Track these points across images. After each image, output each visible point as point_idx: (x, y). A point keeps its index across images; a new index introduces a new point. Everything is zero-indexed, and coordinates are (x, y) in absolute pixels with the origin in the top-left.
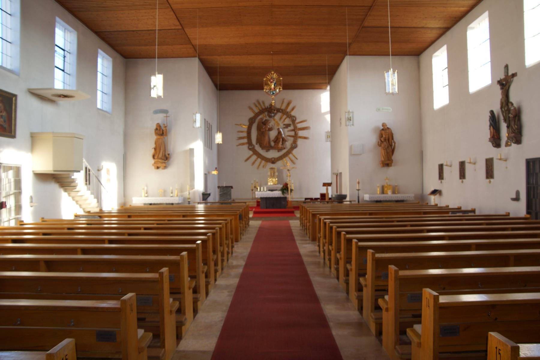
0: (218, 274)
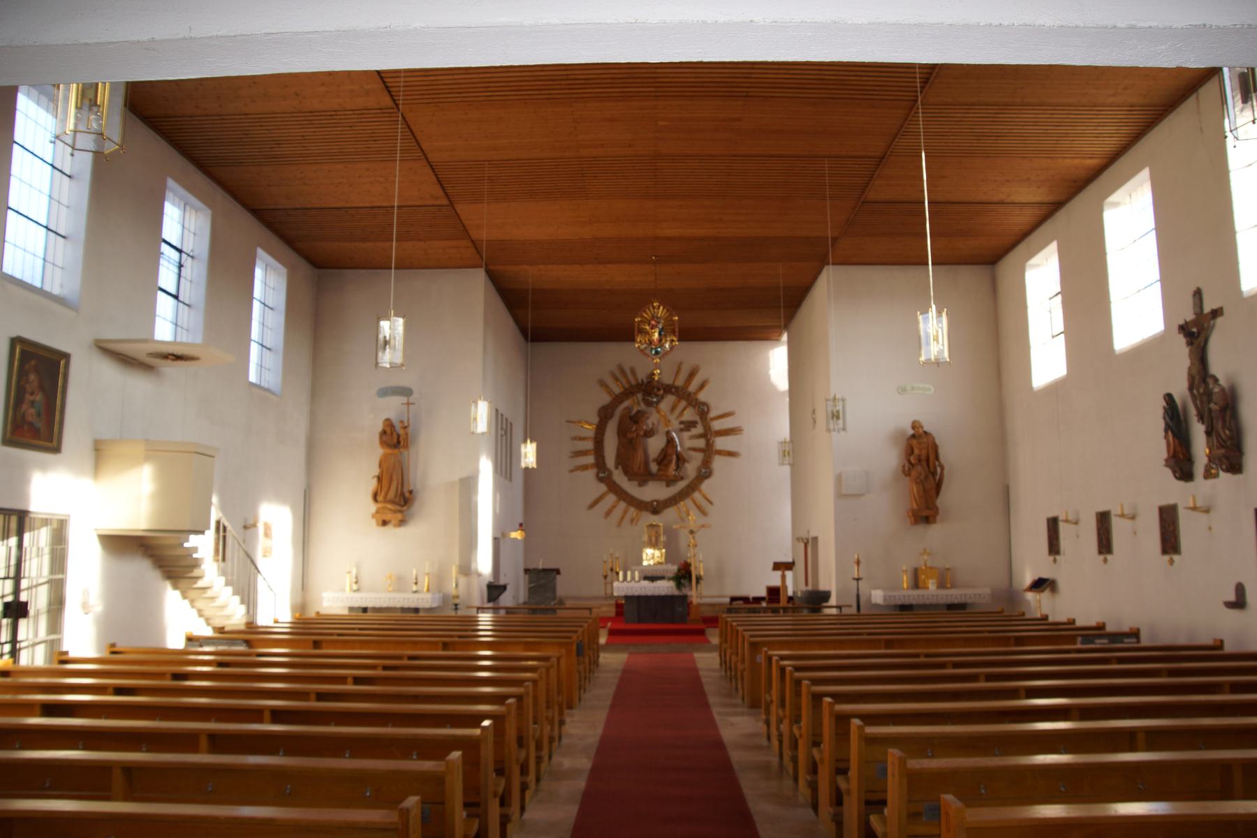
0: (528, 794)
